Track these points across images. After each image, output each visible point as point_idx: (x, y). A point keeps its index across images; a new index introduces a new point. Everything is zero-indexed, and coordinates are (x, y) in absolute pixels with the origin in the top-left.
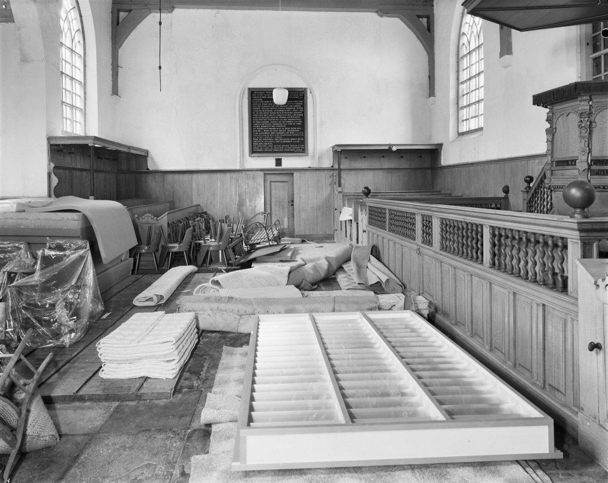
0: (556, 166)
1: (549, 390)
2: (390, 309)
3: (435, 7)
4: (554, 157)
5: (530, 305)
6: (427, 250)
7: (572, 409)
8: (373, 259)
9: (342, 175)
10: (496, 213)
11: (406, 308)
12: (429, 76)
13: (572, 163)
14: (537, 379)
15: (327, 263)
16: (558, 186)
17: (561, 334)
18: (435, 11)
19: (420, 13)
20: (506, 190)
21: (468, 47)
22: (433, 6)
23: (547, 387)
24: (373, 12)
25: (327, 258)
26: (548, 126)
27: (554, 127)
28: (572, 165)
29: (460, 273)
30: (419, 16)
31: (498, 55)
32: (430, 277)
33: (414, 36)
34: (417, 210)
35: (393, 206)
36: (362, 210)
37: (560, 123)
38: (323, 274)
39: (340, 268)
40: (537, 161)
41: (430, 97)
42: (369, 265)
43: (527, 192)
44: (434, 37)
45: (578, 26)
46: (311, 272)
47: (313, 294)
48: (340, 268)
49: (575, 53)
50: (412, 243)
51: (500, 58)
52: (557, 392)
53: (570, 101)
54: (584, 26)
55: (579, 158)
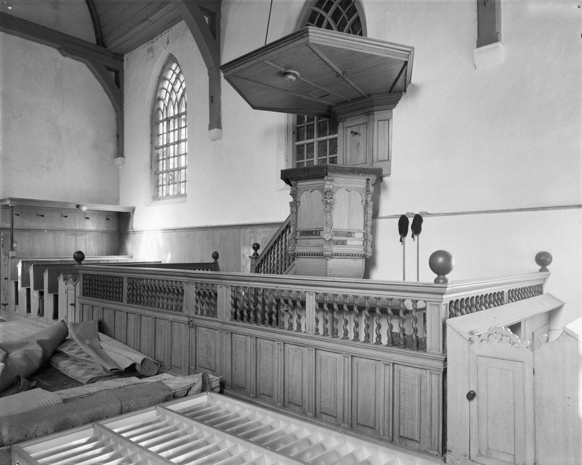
0: (300, 235)
1: (398, 441)
2: (186, 395)
3: (125, 63)
4: (298, 227)
5: (374, 367)
6: (207, 322)
7: (430, 453)
8: (101, 335)
9: (15, 238)
10: (335, 280)
11: (203, 390)
12: (117, 135)
13: (316, 233)
14: (384, 435)
15: (40, 349)
16: (344, 254)
17: (417, 389)
18: (125, 67)
19: (110, 65)
20: (216, 256)
21: (165, 114)
22: (123, 61)
23: (396, 439)
24: (54, 47)
25: (40, 342)
26: (291, 199)
27: (298, 201)
28: (316, 235)
29: (264, 344)
30: (109, 69)
31: (207, 127)
32: (210, 350)
33: (102, 88)
34: (188, 278)
35: (136, 273)
36: (65, 279)
37: (304, 198)
38: (36, 364)
39: (57, 352)
40: (249, 230)
41: (118, 157)
42: (102, 344)
43: (256, 258)
44: (123, 94)
45: (286, 114)
46: (24, 365)
47: (396, 384)
48: (57, 352)
49: (284, 138)
50: (180, 315)
51: (209, 129)
52: (408, 442)
53: (314, 179)
54: (291, 115)
55: (324, 229)
